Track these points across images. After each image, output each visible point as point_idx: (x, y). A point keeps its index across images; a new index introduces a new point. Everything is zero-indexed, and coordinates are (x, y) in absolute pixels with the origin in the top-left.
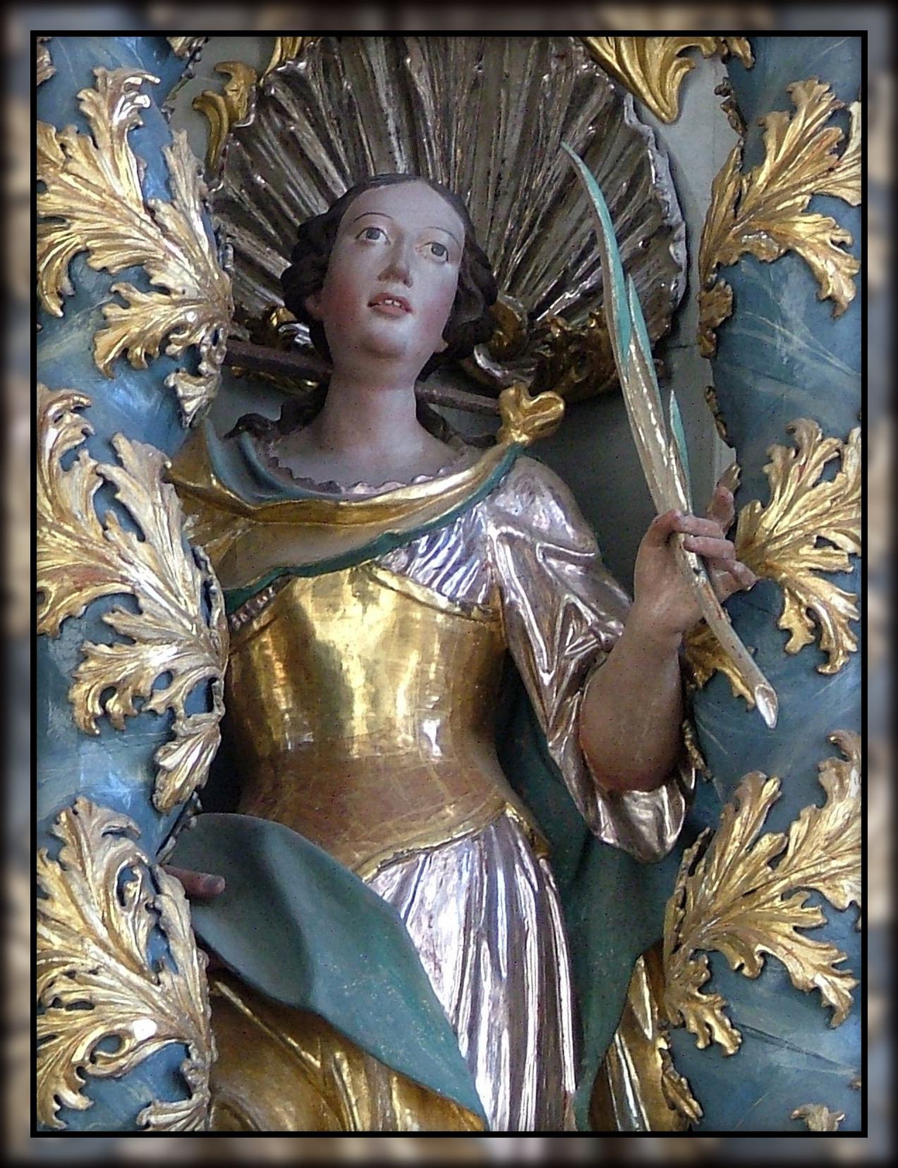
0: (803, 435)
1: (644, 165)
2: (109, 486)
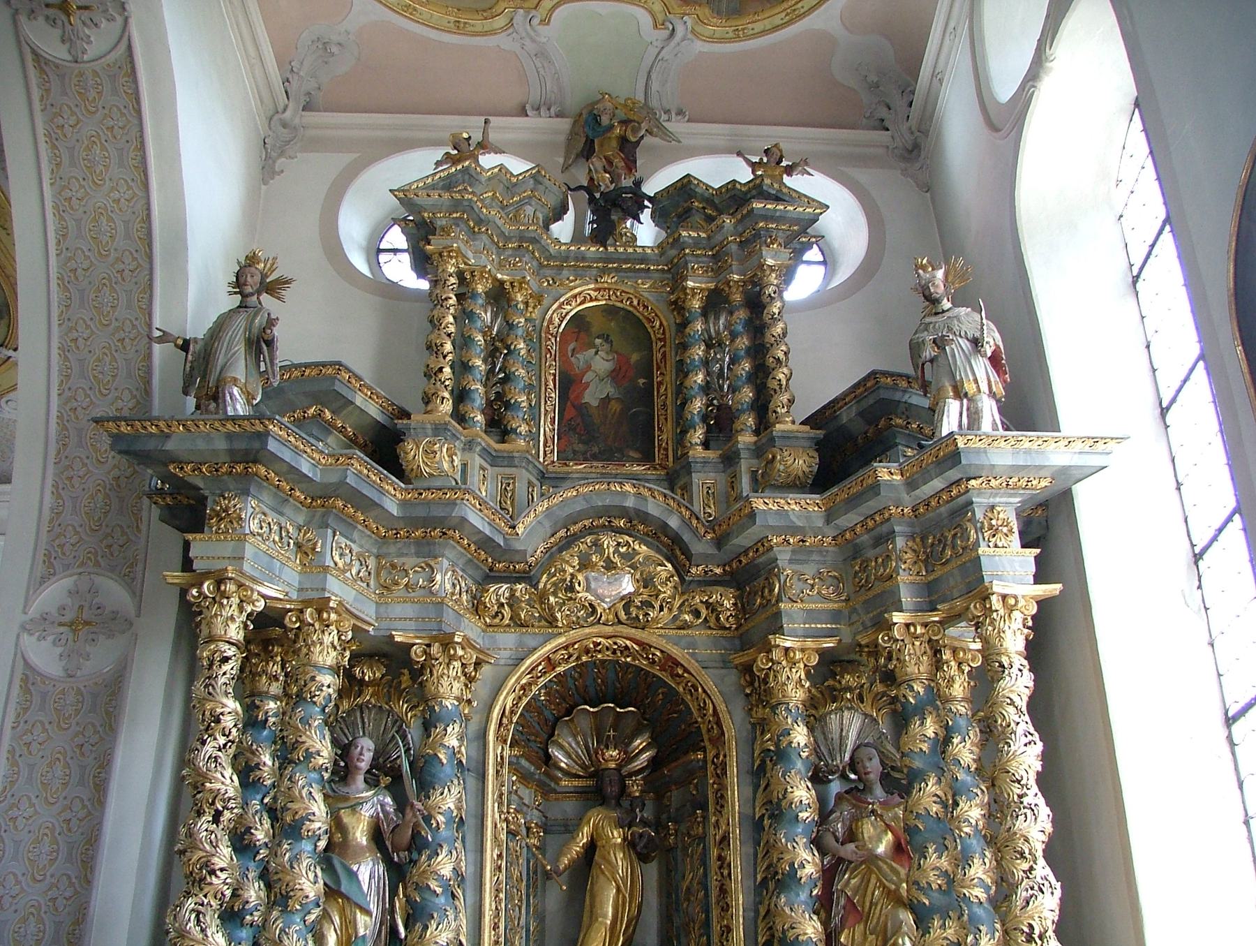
0: (436, 787)
1: (406, 736)
2: (311, 793)
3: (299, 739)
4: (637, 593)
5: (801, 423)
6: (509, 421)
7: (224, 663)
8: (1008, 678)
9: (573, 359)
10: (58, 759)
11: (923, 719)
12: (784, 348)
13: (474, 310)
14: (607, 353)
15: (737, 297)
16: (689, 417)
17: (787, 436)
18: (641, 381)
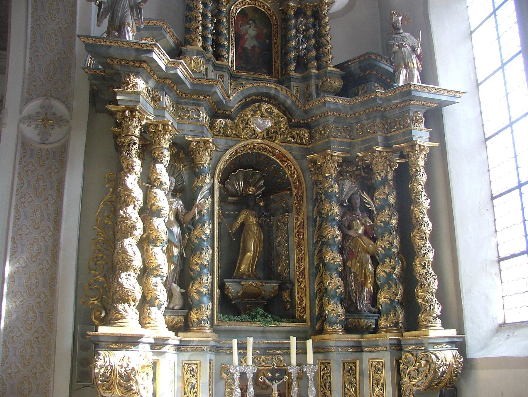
3: (158, 177)
4: (272, 127)
5: (334, 67)
6: (221, 52)
7: (134, 145)
8: (419, 175)
9: (241, 28)
10: (40, 178)
11: (384, 187)
12: (329, 36)
13: (208, 3)
14: (254, 27)
15: (309, 13)
16: (290, 59)
17: (331, 72)
18: (267, 41)
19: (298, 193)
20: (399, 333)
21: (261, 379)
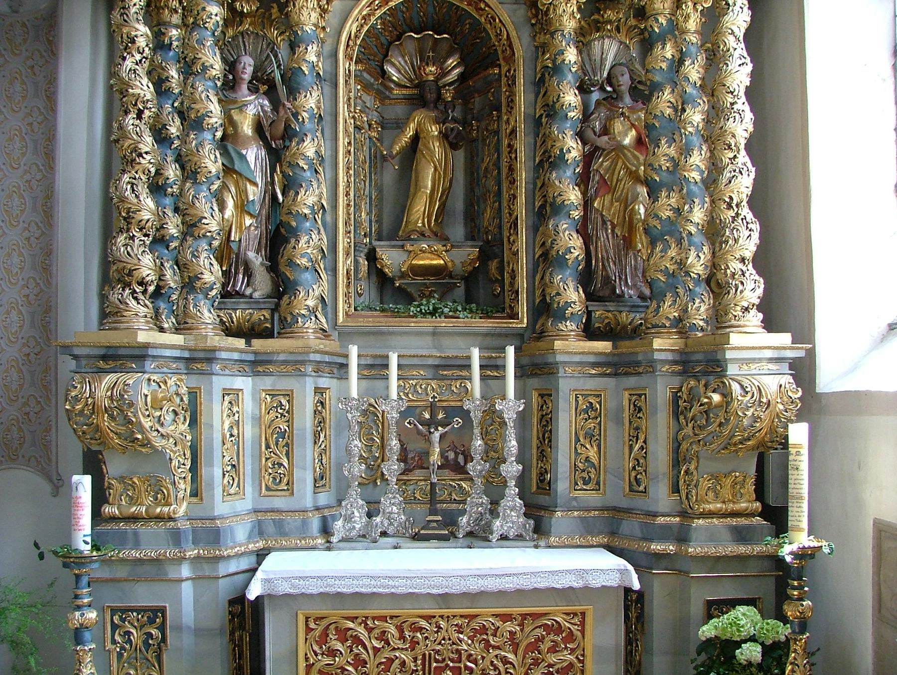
2: (208, 96)
19: (509, 71)
20: (680, 341)
21: (409, 423)
